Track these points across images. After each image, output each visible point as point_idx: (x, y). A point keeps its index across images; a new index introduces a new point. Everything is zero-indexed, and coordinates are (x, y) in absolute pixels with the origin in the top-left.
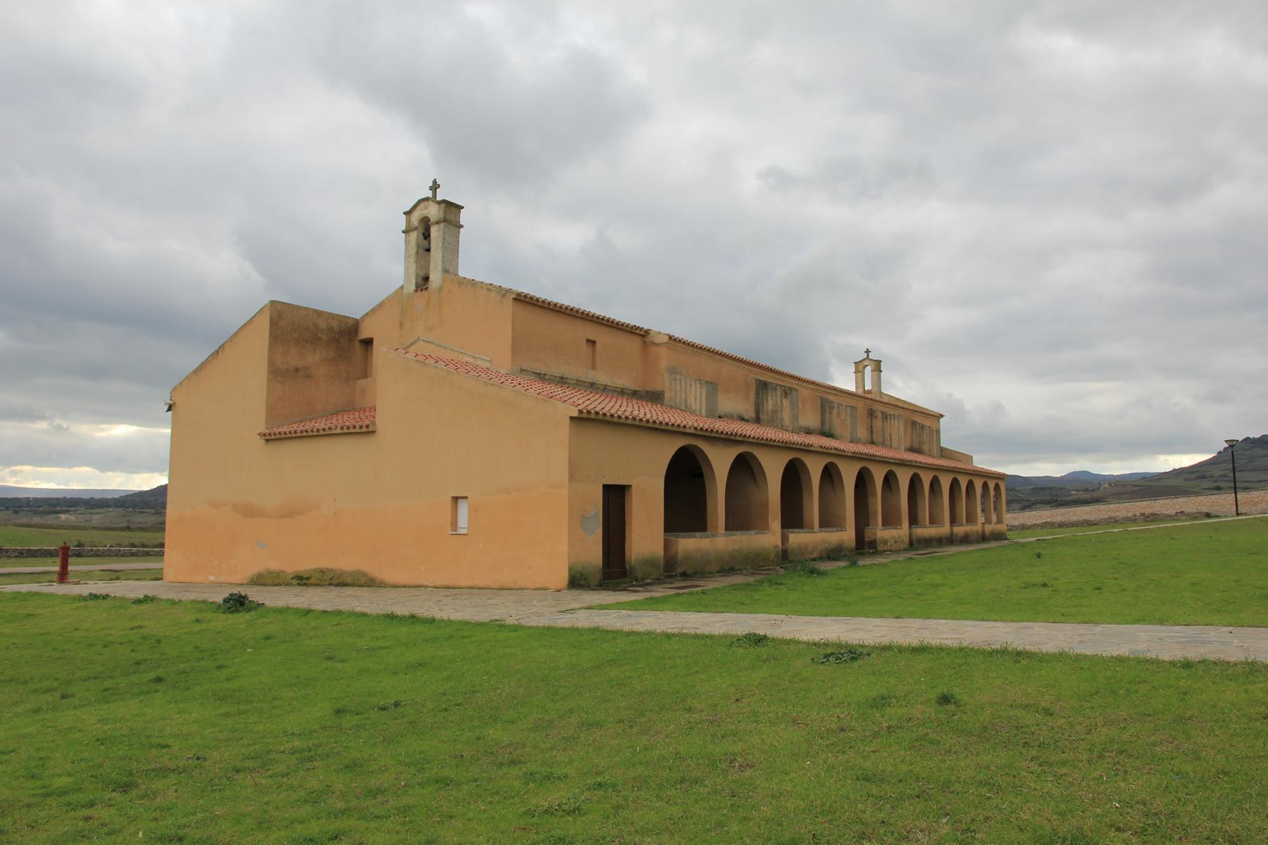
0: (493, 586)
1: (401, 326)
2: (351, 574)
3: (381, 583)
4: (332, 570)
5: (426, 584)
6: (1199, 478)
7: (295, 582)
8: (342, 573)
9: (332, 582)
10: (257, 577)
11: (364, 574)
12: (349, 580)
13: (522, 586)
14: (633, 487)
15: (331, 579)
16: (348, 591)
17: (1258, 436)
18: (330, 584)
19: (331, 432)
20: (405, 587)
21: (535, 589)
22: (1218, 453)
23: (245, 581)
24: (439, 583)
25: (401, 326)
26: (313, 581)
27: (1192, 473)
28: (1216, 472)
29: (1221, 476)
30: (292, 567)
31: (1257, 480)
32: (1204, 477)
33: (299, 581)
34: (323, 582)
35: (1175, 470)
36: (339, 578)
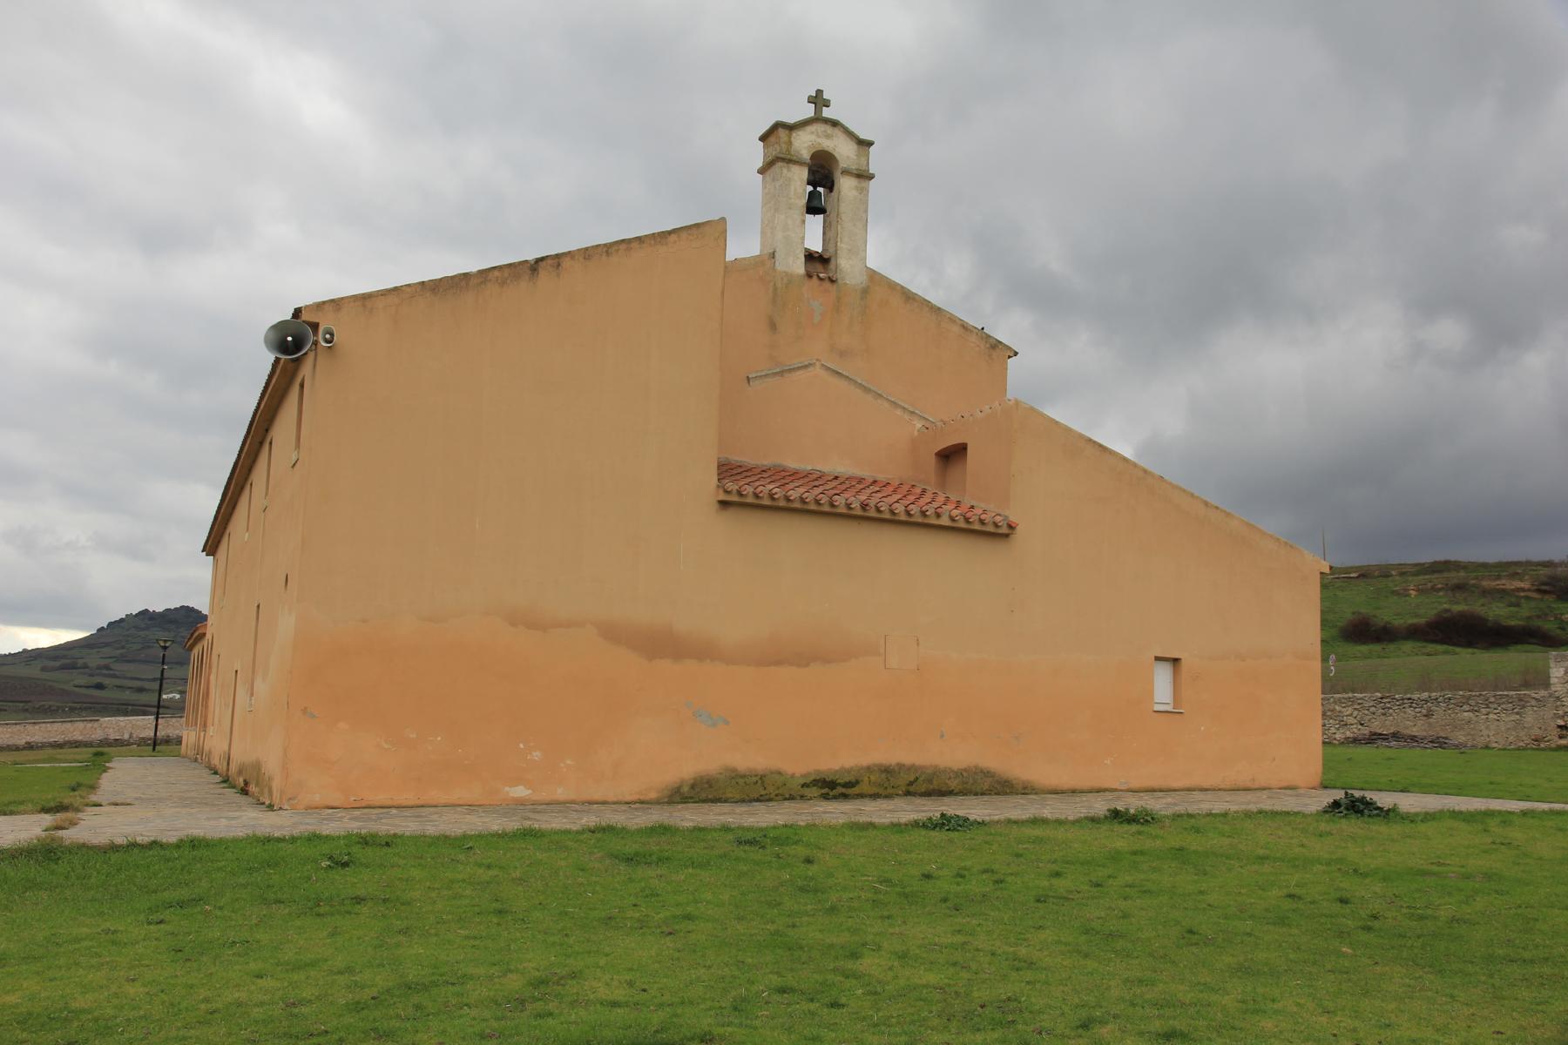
0: (1222, 786)
1: (773, 326)
2: (959, 774)
3: (1025, 788)
4: (911, 768)
5: (1114, 787)
6: (64, 668)
7: (815, 791)
8: (936, 772)
9: (912, 789)
10: (693, 787)
11: (987, 774)
12: (954, 784)
13: (1263, 784)
14: (1183, 660)
15: (911, 784)
16: (946, 800)
17: (159, 609)
18: (908, 793)
19: (926, 521)
20: (1055, 792)
21: (1280, 789)
22: (98, 630)
23: (653, 795)
24: (1135, 784)
25: (773, 326)
26: (864, 788)
27: (56, 658)
28: (94, 660)
29: (99, 667)
30: (799, 766)
31: (151, 677)
32: (73, 667)
33: (826, 790)
34: (890, 791)
35: (25, 651)
36: (930, 781)
